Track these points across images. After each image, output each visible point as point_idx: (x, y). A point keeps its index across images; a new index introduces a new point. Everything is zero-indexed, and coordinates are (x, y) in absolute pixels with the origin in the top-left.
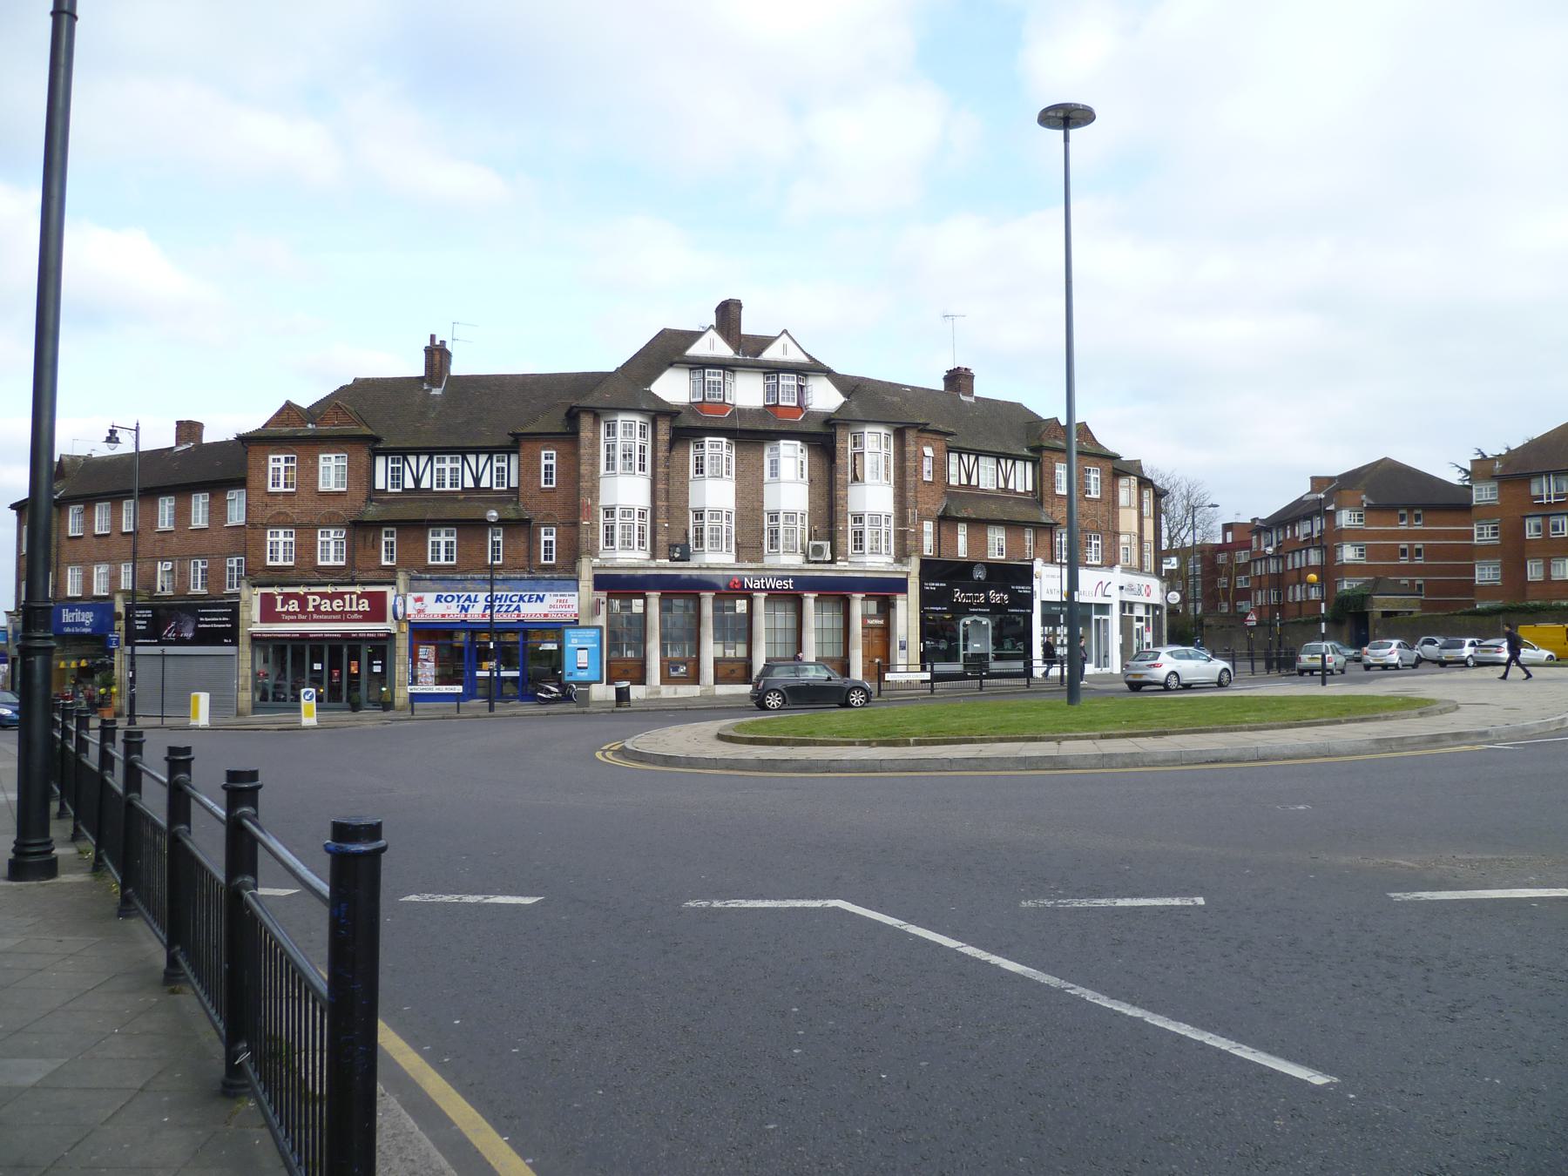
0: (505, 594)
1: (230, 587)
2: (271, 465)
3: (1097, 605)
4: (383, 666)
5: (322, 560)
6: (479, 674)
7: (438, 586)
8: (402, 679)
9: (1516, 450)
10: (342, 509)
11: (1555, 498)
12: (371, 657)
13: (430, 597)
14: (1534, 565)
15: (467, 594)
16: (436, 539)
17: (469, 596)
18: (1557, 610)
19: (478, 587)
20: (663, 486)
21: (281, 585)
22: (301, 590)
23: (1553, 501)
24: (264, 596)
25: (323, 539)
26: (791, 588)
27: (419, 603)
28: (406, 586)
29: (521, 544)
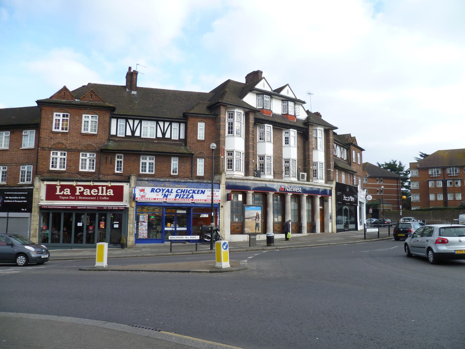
0: (186, 189)
1: (21, 181)
2: (55, 118)
4: (120, 225)
5: (82, 168)
6: (166, 229)
7: (151, 184)
8: (131, 231)
10: (95, 143)
11: (437, 175)
12: (113, 220)
13: (148, 189)
14: (450, 195)
15: (167, 189)
16: (144, 161)
17: (168, 190)
18: (451, 209)
19: (172, 185)
20: (252, 143)
21: (61, 180)
22: (74, 184)
23: (436, 176)
24: (48, 186)
25: (83, 158)
27: (142, 192)
28: (135, 184)
29: (188, 166)
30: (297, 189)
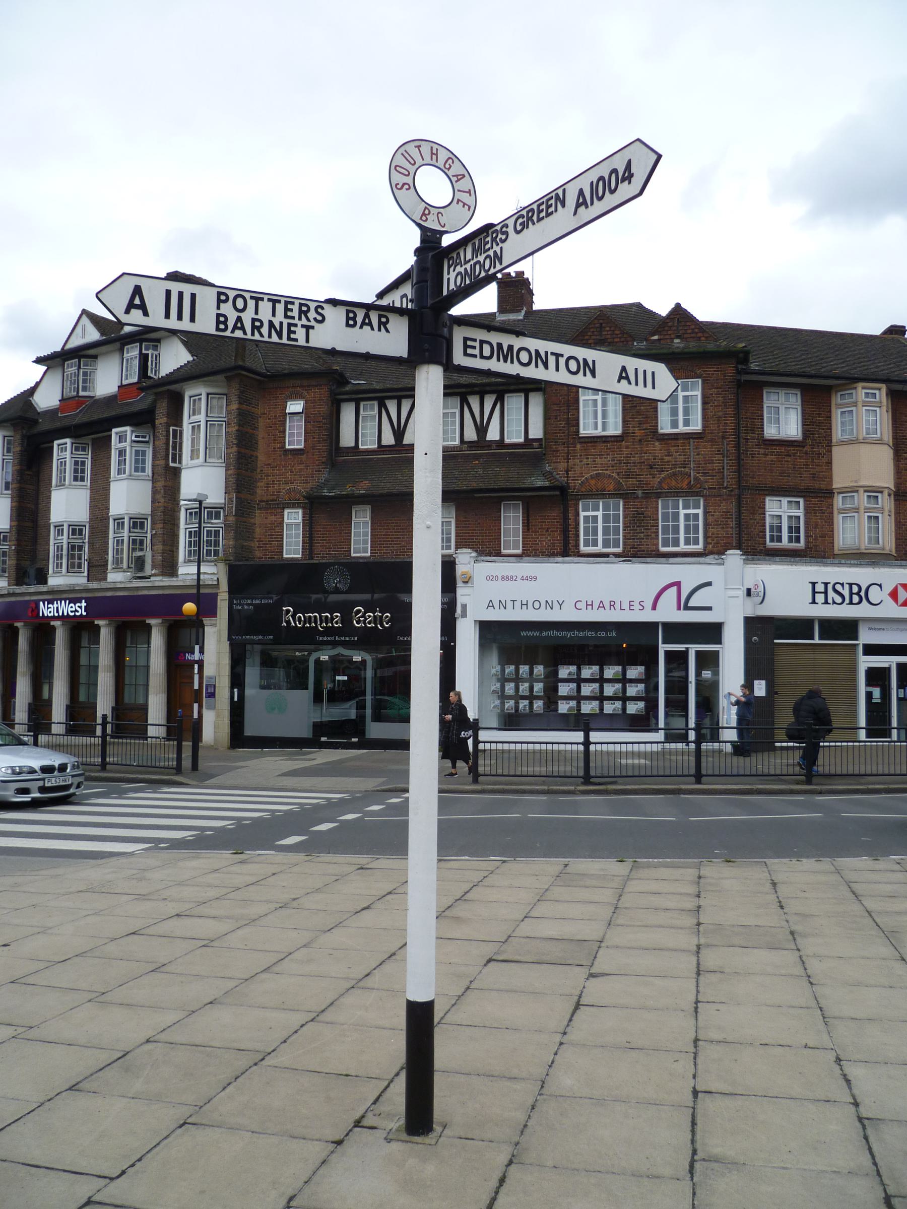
3: (666, 625)
9: (667, 315)
26: (84, 614)
30: (72, 607)
